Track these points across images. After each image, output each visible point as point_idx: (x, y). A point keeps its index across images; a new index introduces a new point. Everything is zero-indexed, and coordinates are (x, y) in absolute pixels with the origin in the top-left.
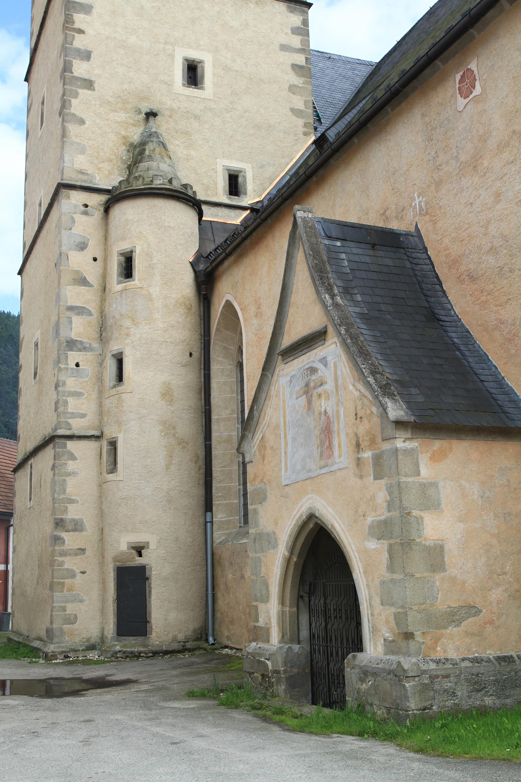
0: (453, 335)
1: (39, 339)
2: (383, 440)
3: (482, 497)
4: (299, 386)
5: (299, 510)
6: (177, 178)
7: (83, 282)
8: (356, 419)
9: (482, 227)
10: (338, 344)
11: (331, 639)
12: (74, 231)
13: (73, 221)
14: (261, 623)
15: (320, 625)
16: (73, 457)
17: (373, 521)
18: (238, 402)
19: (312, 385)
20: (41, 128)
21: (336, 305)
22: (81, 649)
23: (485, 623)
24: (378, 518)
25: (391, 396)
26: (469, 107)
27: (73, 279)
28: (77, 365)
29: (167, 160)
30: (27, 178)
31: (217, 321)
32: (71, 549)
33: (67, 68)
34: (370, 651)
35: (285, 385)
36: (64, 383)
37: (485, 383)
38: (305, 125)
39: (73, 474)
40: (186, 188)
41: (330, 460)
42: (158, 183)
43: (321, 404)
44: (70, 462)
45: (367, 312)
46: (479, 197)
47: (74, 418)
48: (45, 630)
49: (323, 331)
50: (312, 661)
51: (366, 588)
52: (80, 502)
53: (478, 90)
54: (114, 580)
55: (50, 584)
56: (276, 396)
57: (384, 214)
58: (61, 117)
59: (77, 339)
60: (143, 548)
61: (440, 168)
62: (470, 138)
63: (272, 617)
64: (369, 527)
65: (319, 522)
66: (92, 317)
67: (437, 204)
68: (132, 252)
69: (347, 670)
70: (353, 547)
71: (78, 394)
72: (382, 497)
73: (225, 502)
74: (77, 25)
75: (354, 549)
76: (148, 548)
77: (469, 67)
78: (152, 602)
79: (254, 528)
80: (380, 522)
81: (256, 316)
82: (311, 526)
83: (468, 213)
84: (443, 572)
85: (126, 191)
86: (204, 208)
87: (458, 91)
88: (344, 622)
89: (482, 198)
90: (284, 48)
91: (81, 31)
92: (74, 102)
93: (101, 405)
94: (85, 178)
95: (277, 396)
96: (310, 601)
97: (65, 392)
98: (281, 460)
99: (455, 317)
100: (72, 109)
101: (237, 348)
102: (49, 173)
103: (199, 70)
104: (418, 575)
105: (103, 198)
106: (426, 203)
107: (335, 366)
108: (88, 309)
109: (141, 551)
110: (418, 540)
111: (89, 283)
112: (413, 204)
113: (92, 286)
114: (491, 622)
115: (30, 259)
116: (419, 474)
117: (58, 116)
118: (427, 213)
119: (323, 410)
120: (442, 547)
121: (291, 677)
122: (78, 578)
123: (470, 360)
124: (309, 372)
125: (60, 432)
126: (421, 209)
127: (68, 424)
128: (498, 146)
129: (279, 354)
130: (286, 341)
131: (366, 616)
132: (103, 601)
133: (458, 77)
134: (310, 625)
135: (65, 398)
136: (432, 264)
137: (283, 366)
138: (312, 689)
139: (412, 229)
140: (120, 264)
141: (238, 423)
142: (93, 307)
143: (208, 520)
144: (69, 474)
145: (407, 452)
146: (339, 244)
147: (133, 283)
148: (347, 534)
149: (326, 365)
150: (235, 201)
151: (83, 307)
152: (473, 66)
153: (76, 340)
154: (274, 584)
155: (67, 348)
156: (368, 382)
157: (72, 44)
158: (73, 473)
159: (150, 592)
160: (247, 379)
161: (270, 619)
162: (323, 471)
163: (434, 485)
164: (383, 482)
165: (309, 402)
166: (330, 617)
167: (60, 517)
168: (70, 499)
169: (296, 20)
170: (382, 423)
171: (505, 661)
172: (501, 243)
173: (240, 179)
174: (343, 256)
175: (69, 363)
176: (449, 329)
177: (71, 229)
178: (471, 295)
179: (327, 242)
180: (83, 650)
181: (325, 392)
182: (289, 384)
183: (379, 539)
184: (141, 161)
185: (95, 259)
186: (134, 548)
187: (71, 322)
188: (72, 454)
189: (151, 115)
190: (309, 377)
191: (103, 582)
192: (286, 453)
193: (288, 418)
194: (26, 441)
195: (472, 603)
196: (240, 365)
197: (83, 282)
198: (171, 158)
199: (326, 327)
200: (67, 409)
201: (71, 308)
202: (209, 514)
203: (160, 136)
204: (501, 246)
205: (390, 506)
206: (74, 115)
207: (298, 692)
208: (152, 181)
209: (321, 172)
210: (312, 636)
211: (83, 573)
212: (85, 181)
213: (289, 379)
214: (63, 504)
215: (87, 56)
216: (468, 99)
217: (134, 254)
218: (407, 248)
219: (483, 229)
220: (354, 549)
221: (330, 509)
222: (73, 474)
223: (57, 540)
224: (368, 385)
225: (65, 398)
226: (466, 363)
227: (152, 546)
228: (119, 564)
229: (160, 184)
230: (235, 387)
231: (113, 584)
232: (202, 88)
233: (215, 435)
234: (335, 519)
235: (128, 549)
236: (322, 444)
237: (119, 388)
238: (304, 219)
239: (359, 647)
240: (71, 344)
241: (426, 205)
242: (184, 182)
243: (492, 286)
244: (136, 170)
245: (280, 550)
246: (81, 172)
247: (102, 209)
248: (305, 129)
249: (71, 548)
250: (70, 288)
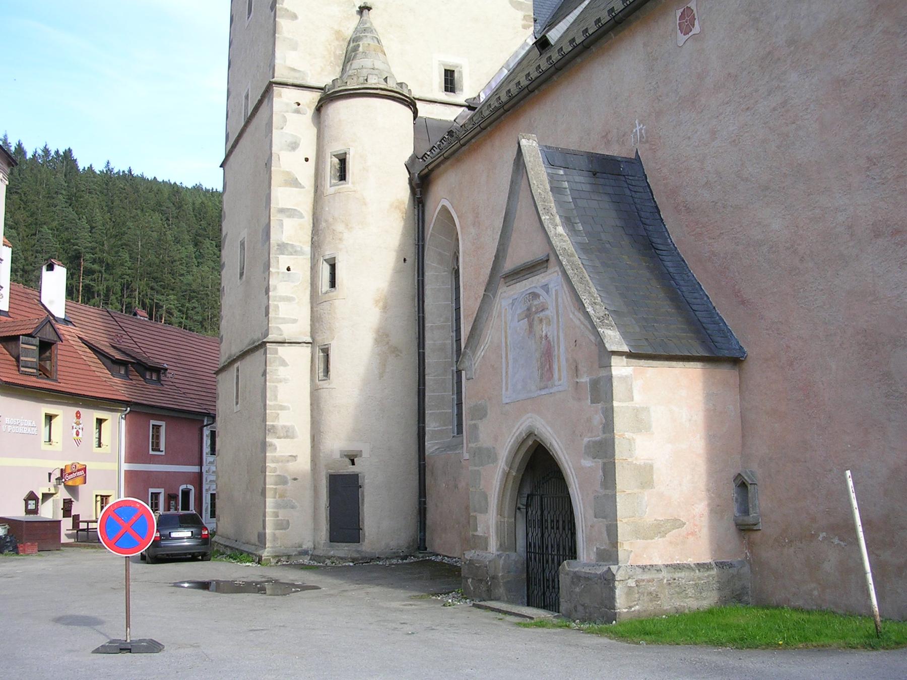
0: (669, 264)
1: (246, 238)
2: (600, 367)
3: (690, 420)
4: (520, 309)
5: (519, 428)
6: (393, 77)
7: (294, 183)
8: (576, 345)
9: (698, 161)
10: (560, 273)
11: (547, 548)
14: (480, 532)
15: (537, 535)
16: (284, 363)
17: (589, 442)
18: (452, 310)
19: (534, 310)
20: (248, 18)
22: (294, 554)
23: (688, 534)
24: (593, 439)
26: (688, 43)
27: (285, 180)
28: (288, 269)
29: (380, 54)
30: (231, 66)
31: (432, 226)
32: (283, 456)
34: (583, 558)
35: (507, 307)
37: (697, 313)
38: (525, 18)
39: (285, 380)
40: (401, 87)
41: (549, 383)
42: (373, 81)
43: (542, 329)
44: (281, 369)
45: (588, 242)
46: (696, 132)
47: (285, 323)
48: (257, 535)
49: (545, 259)
50: (528, 567)
51: (581, 501)
52: (291, 409)
53: (696, 29)
54: (327, 487)
55: (262, 490)
56: (498, 316)
57: (605, 136)
58: (273, 12)
59: (289, 242)
60: (356, 456)
61: (660, 99)
62: (688, 74)
63: (491, 526)
64: (585, 446)
65: (538, 440)
66: (302, 220)
67: (657, 133)
68: (346, 153)
69: (562, 577)
70: (570, 464)
71: (288, 299)
73: (438, 411)
75: (571, 466)
76: (361, 456)
77: (688, 6)
78: (365, 510)
79: (475, 442)
80: (595, 442)
81: (474, 224)
82: (530, 443)
83: (686, 146)
84: (652, 488)
85: (340, 91)
86: (419, 105)
87: (678, 27)
88: (561, 533)
89: (699, 133)
94: (297, 75)
95: (499, 316)
96: (527, 512)
97: (276, 297)
98: (502, 379)
99: (672, 246)
100: (284, 4)
101: (452, 254)
102: (258, 66)
104: (628, 491)
105: (316, 96)
106: (647, 131)
107: (557, 295)
108: (299, 212)
109: (353, 460)
111: (300, 184)
112: (634, 131)
113: (303, 187)
114: (693, 534)
115: (234, 153)
117: (269, 9)
118: (647, 142)
120: (651, 466)
121: (508, 582)
122: (289, 484)
123: (684, 289)
124: (531, 297)
127: (279, 329)
128: (715, 86)
130: (509, 265)
131: (581, 526)
132: (316, 509)
134: (527, 535)
135: (276, 303)
137: (505, 288)
138: (528, 593)
141: (452, 332)
144: (280, 381)
146: (561, 172)
147: (346, 186)
148: (565, 452)
149: (547, 292)
151: (295, 210)
153: (287, 244)
154: (493, 496)
155: (278, 252)
158: (284, 379)
159: (363, 500)
160: (464, 288)
161: (488, 528)
162: (543, 392)
163: (646, 409)
164: (600, 406)
165: (531, 325)
166: (547, 528)
167: (271, 423)
168: (281, 406)
170: (600, 351)
171: (704, 568)
172: (716, 179)
173: (456, 75)
175: (280, 267)
176: (665, 258)
177: (282, 128)
178: (687, 226)
180: (295, 555)
181: (546, 317)
182: (511, 306)
185: (307, 160)
186: (347, 456)
187: (282, 224)
188: (284, 361)
190: (531, 302)
192: (507, 372)
193: (509, 339)
194: (231, 343)
195: (676, 517)
196: (457, 272)
197: (294, 183)
198: (385, 55)
199: (548, 255)
200: (278, 314)
201: (282, 211)
203: (374, 31)
204: (715, 182)
207: (514, 596)
209: (543, 87)
210: (529, 545)
212: (297, 78)
213: (511, 301)
214: (274, 410)
216: (687, 37)
217: (347, 156)
218: (628, 176)
219: (700, 164)
220: (571, 466)
221: (549, 429)
225: (276, 303)
226: (680, 292)
227: (365, 454)
228: (332, 471)
229: (374, 84)
230: (451, 295)
231: (325, 491)
233: (428, 342)
234: (554, 438)
235: (341, 457)
236: (542, 367)
239: (573, 554)
241: (646, 134)
243: (706, 219)
244: (350, 68)
245: (499, 465)
248: (523, 22)
249: (283, 454)
250: (281, 189)
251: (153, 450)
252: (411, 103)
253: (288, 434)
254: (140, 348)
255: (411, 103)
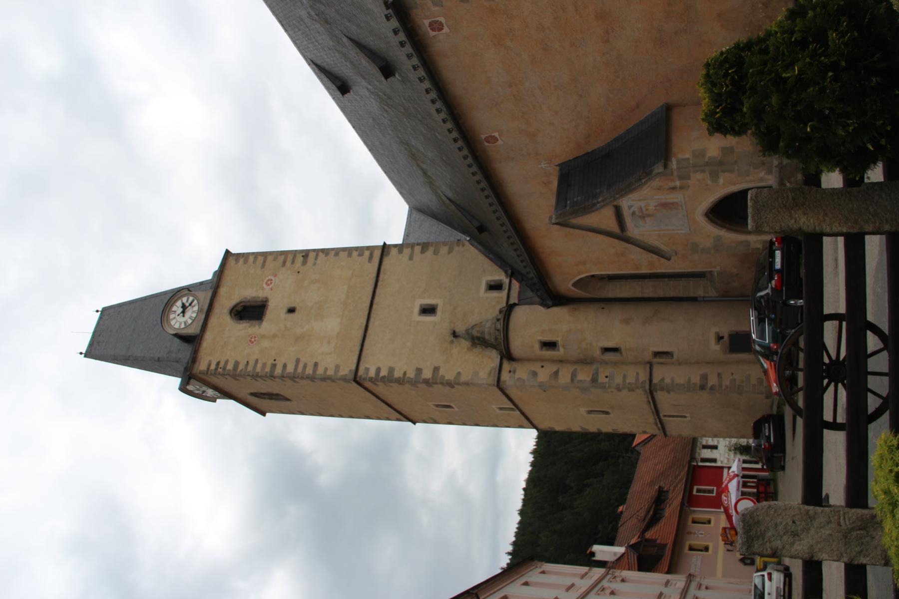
7: (556, 374)
12: (525, 378)
13: (519, 379)
14: (760, 246)
16: (663, 380)
21: (603, 201)
25: (651, 171)
28: (607, 377)
33: (427, 382)
36: (618, 385)
39: (673, 379)
42: (499, 326)
44: (665, 381)
53: (496, 134)
60: (718, 336)
71: (625, 377)
72: (699, 176)
74: (401, 375)
85: (505, 348)
86: (512, 301)
90: (411, 258)
91: (405, 373)
92: (447, 378)
93: (632, 363)
103: (426, 307)
110: (719, 158)
113: (558, 369)
116: (688, 159)
119: (654, 208)
125: (647, 386)
126: (548, 163)
127: (642, 383)
129: (622, 233)
133: (486, 144)
136: (577, 157)
139: (558, 168)
140: (547, 350)
142: (571, 368)
143: (702, 299)
144: (673, 382)
145: (679, 162)
146: (569, 202)
147: (559, 341)
150: (506, 286)
152: (483, 137)
156: (645, 182)
157: (412, 379)
162: (684, 207)
165: (649, 216)
169: (394, 252)
173: (492, 283)
174: (575, 199)
179: (568, 208)
183: (718, 177)
184: (484, 338)
185: (542, 367)
189: (455, 335)
191: (739, 362)
197: (556, 374)
201: (572, 380)
202: (699, 299)
205: (704, 171)
206: (455, 378)
208: (498, 330)
211: (732, 374)
215: (419, 371)
216: (499, 139)
222: (673, 379)
223: (712, 388)
224: (646, 183)
227: (717, 330)
232: (437, 305)
233: (651, 295)
237: (623, 350)
238: (556, 219)
240: (594, 380)
242: (498, 313)
246: (490, 374)
247: (512, 362)
250: (559, 381)
251: (713, 493)
252: (510, 308)
253: (704, 377)
254: (645, 505)
255: (510, 308)
